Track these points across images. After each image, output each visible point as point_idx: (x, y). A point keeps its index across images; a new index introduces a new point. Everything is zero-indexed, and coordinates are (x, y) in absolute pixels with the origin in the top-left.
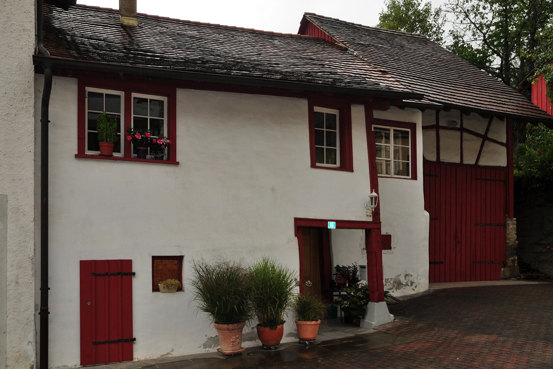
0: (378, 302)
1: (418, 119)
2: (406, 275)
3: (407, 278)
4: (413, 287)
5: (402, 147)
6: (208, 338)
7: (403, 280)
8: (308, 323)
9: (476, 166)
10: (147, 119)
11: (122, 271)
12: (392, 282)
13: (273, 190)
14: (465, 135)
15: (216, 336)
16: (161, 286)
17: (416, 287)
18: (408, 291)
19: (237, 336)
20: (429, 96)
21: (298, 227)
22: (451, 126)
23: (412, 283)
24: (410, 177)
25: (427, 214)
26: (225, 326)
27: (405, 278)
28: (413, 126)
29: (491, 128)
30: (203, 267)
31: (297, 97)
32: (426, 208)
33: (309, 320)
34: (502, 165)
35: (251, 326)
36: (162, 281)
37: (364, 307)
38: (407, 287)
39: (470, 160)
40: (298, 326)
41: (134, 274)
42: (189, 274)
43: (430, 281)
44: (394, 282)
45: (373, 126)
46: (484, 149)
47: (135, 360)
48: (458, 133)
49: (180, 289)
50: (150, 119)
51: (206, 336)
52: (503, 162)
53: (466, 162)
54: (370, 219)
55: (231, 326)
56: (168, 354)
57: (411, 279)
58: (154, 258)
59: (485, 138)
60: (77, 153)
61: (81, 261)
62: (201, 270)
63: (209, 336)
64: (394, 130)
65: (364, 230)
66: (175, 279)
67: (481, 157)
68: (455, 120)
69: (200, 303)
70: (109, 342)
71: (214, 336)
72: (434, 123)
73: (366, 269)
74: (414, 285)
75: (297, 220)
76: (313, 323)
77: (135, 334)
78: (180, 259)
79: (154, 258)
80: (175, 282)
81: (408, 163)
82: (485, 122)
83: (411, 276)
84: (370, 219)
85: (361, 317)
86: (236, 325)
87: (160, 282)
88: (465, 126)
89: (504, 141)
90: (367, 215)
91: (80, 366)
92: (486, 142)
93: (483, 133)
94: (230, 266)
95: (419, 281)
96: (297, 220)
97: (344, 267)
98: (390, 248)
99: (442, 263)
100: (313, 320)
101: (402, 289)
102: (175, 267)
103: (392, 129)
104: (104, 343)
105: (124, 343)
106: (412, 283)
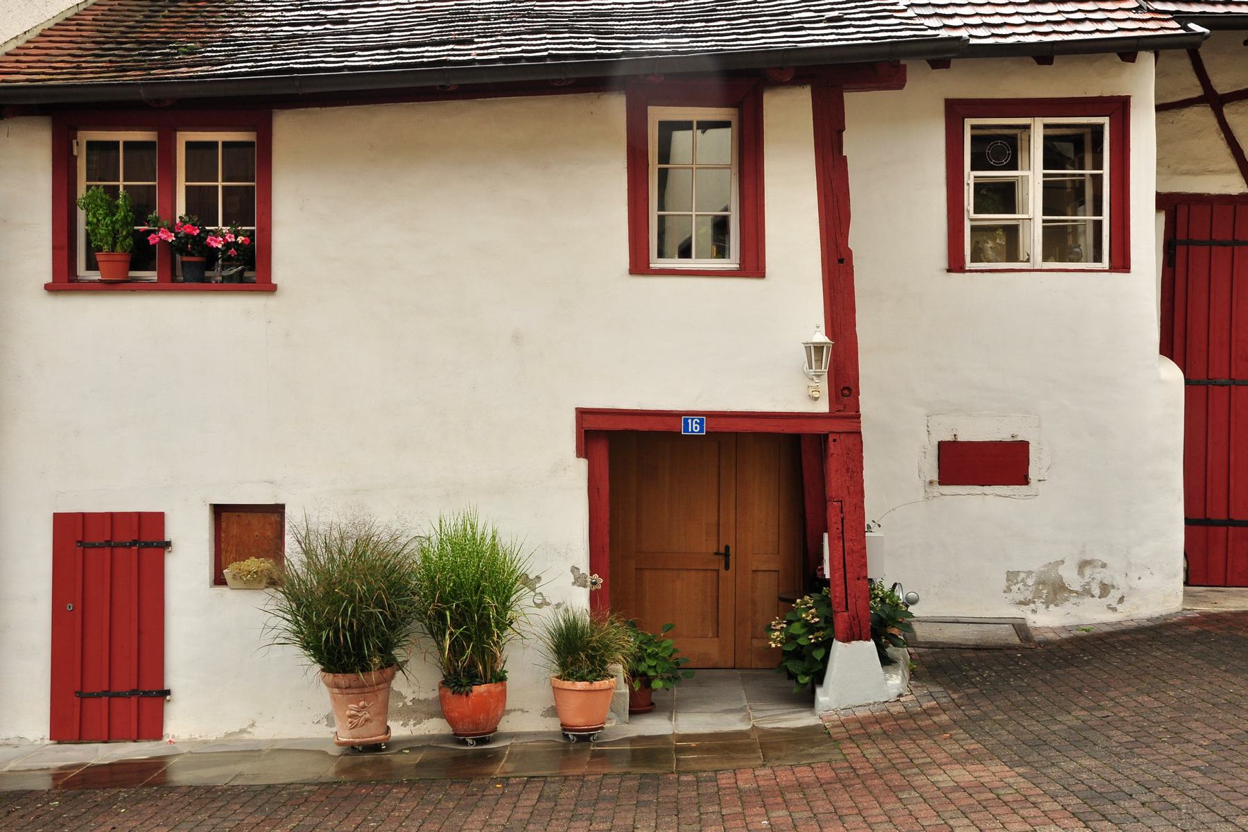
1: (1141, 84)
2: (1084, 565)
3: (1088, 571)
5: (1092, 175)
10: (223, 181)
11: (142, 537)
12: (1030, 582)
13: (517, 338)
17: (1121, 600)
18: (1094, 615)
19: (362, 704)
20: (856, 7)
23: (1105, 589)
24: (1105, 263)
25: (1172, 374)
28: (1119, 108)
31: (595, 91)
35: (417, 677)
38: (1088, 599)
41: (169, 544)
43: (1190, 580)
44: (1041, 582)
45: (969, 122)
47: (166, 739)
50: (223, 187)
56: (242, 731)
57: (1100, 575)
58: (219, 511)
60: (49, 280)
61: (56, 515)
70: (111, 695)
74: (1114, 595)
75: (582, 414)
77: (173, 679)
79: (219, 511)
80: (265, 564)
83: (1104, 566)
91: (48, 741)
94: (394, 529)
95: (1135, 583)
96: (582, 414)
98: (1025, 481)
100: (582, 679)
104: (99, 696)
105: (144, 701)
106: (1105, 589)
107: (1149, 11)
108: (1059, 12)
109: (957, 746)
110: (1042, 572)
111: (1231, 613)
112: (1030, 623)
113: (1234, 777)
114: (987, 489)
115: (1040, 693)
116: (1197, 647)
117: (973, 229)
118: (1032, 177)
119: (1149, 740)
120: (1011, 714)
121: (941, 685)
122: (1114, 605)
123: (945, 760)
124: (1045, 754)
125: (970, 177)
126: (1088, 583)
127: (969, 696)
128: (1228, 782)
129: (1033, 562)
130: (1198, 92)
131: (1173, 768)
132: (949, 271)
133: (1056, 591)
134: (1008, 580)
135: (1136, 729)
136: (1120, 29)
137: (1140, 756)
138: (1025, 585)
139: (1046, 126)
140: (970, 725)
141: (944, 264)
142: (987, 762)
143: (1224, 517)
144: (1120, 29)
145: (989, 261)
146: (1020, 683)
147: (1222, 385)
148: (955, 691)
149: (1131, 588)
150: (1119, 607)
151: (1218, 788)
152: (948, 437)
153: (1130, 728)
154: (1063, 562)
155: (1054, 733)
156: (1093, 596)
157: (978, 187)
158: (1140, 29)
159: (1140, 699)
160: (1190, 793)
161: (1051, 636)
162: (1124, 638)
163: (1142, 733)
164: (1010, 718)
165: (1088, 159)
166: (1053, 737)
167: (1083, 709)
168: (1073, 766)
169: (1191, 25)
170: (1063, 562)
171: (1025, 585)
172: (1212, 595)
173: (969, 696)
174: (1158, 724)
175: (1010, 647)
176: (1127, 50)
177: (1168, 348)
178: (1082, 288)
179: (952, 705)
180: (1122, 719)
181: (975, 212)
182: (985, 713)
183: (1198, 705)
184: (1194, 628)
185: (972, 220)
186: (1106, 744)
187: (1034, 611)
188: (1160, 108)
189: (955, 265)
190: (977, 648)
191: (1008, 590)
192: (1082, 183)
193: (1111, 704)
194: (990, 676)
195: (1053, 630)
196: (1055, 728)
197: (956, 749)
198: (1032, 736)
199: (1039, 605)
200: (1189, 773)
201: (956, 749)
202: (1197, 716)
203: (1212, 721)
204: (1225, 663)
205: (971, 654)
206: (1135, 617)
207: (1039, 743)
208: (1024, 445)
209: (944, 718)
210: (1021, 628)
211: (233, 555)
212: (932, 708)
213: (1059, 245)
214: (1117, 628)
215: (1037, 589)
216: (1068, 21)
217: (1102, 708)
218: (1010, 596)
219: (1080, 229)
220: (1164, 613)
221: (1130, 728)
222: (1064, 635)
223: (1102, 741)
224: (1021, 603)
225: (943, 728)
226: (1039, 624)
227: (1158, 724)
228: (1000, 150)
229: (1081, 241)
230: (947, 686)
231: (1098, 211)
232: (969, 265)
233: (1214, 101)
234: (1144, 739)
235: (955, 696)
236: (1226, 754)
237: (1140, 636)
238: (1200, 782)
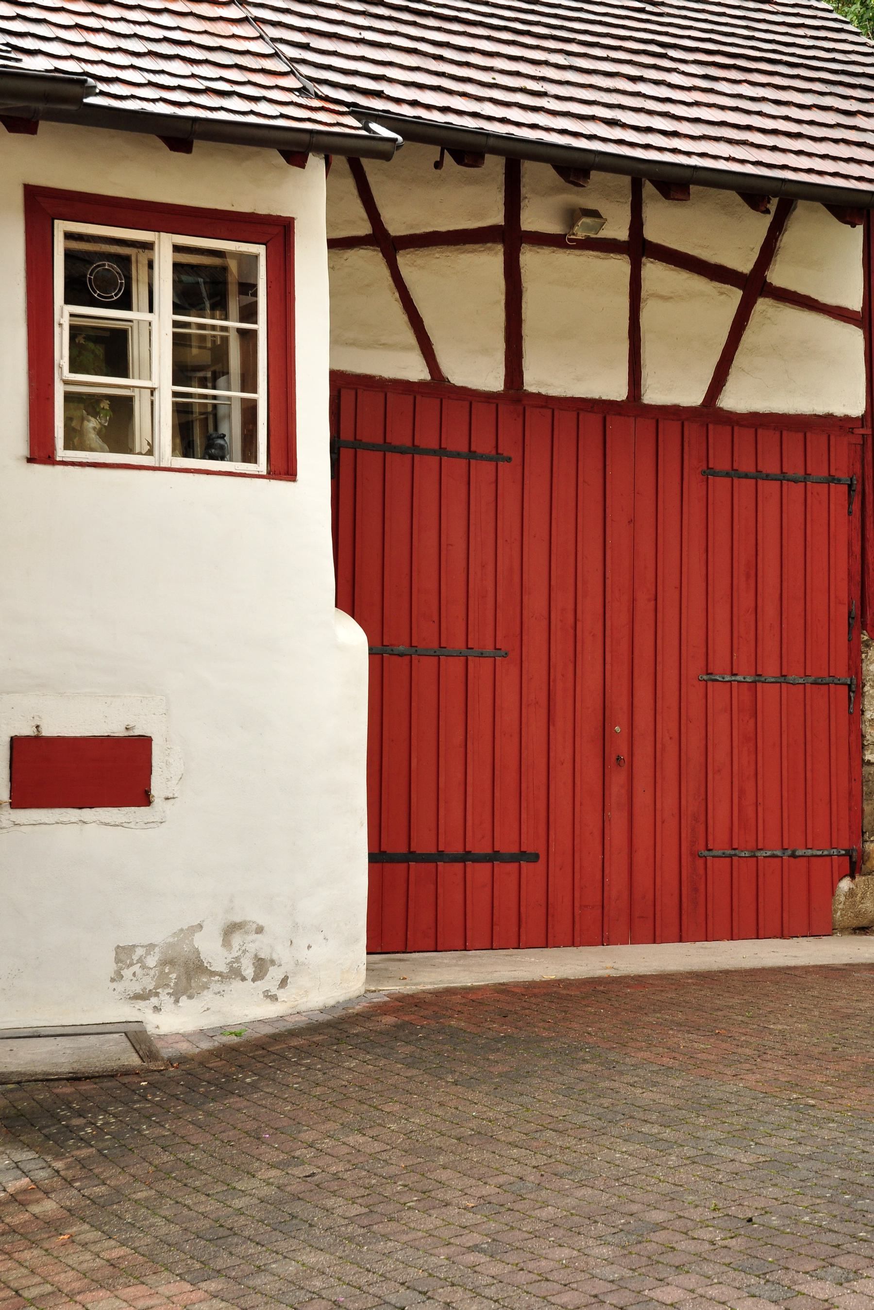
1: (309, 200)
2: (231, 929)
3: (237, 940)
4: (270, 982)
7: (211, 949)
9: (709, 412)
12: (152, 961)
14: (654, 273)
17: (284, 982)
18: (245, 1008)
20: (379, 94)
22: (580, 233)
23: (261, 966)
24: (262, 465)
25: (352, 637)
27: (226, 943)
28: (278, 233)
29: (788, 239)
34: (839, 410)
38: (237, 984)
39: (675, 386)
44: (167, 962)
45: (61, 227)
46: (748, 338)
48: (621, 266)
52: (849, 398)
53: (652, 396)
57: (256, 945)
59: (754, 286)
64: (177, 249)
67: (733, 371)
68: (591, 205)
72: (497, 218)
74: (274, 974)
82: (758, 226)
83: (260, 930)
88: (652, 233)
89: (855, 301)
92: (763, 305)
93: (745, 266)
98: (145, 799)
99: (534, 858)
101: (207, 995)
103: (164, 247)
106: (261, 966)
107: (317, 97)
108: (193, 76)
109: (88, 1256)
110: (170, 945)
111: (430, 992)
112: (150, 1029)
113: (535, 1257)
114: (87, 814)
115: (195, 1146)
116: (403, 1050)
117: (69, 397)
118: (155, 327)
119: (390, 1208)
120: (160, 1186)
121: (30, 1147)
122: (274, 991)
123: (77, 1285)
124: (241, 1250)
125: (63, 313)
126: (237, 959)
127: (82, 1163)
128: (531, 1265)
129: (155, 930)
130: (364, 229)
131: (443, 1252)
132: (30, 460)
133: (188, 974)
134: (118, 960)
135: (363, 1192)
136: (282, 116)
137: (386, 1237)
138: (144, 967)
139: (177, 249)
140: (98, 1212)
141: (22, 448)
142: (151, 1279)
143: (403, 850)
144: (282, 116)
145: (92, 450)
146: (158, 1131)
147: (400, 655)
148: (58, 1156)
149: (297, 963)
150: (281, 994)
151: (522, 1278)
152: (27, 730)
153: (352, 1191)
154: (200, 926)
155: (240, 1212)
156: (244, 979)
157: (75, 331)
158: (309, 120)
159: (351, 1140)
160: (487, 1292)
161: (184, 1047)
162: (294, 1042)
163: (375, 1198)
164: (161, 1194)
165: (233, 307)
166: (242, 1220)
167: (272, 1166)
168: (292, 1268)
169: (374, 126)
170: (200, 926)
171: (144, 967)
172: (393, 966)
173: (82, 1163)
174: (393, 1178)
175: (127, 1072)
176: (295, 148)
177: (348, 599)
178: (226, 498)
179: (57, 1182)
180: (336, 1177)
181: (73, 369)
182: (117, 1190)
183: (437, 1142)
184: (390, 1020)
185: (66, 383)
186: (328, 1223)
187: (157, 1009)
188: (333, 244)
189: (40, 452)
190: (75, 1078)
191: (118, 977)
192: (225, 340)
193: (310, 1154)
194: (107, 1123)
195: (185, 1037)
196: (238, 1203)
197: (85, 1260)
198: (207, 1223)
199: (165, 999)
200: (471, 1258)
201: (85, 1260)
202: (442, 1159)
203: (465, 1165)
204: (453, 1072)
205: (66, 1089)
206: (302, 1008)
207: (222, 1235)
208: (145, 742)
209: (48, 1207)
210: (137, 1038)
212: (25, 1191)
213: (198, 434)
214: (281, 1027)
215: (162, 972)
216: (207, 91)
217: (299, 1161)
218: (120, 986)
219: (222, 411)
220: (341, 999)
221: (352, 1191)
222: (206, 1045)
223: (318, 1216)
224: (138, 997)
225: (53, 1226)
226: (164, 1030)
227: (393, 1178)
228: (102, 278)
229: (224, 429)
230: (41, 1149)
231: (249, 382)
232: (61, 453)
233: (388, 245)
234: (380, 1208)
235: (59, 1165)
236: (507, 1218)
237: (318, 1038)
238: (493, 1271)
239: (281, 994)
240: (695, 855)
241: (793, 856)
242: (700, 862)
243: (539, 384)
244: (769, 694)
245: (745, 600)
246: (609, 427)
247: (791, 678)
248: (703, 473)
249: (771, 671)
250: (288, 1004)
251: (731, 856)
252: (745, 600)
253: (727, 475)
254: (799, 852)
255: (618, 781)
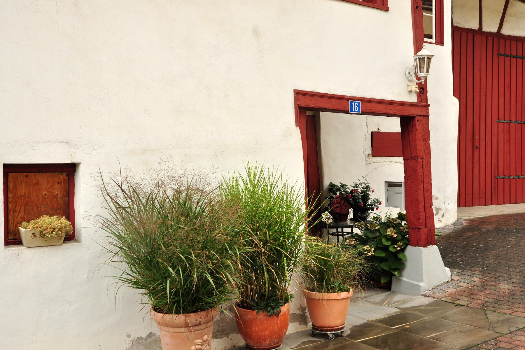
0: (425, 246)
6: (133, 341)
8: (334, 296)
9: (498, 35)
13: (256, 32)
15: (150, 335)
16: (24, 231)
17: (443, 216)
21: (300, 108)
24: (434, 40)
25: (456, 101)
26: (180, 318)
30: (125, 187)
32: (457, 92)
33: (333, 290)
36: (29, 221)
37: (400, 256)
39: (490, 26)
40: (310, 300)
42: (88, 202)
46: (508, 11)
49: (70, 237)
51: (129, 336)
53: (485, 29)
54: (414, 99)
55: (193, 318)
58: (8, 168)
62: (120, 194)
63: (134, 336)
65: (398, 119)
66: (60, 215)
67: (504, 24)
69: (122, 267)
71: (144, 334)
73: (402, 189)
76: (343, 295)
78: (69, 170)
80: (57, 222)
81: (431, 17)
84: (414, 99)
85: (396, 273)
86: (203, 314)
87: (24, 223)
90: (410, 92)
97: (343, 186)
100: (341, 290)
102: (58, 191)
152: (376, 130)
211: (22, 214)
239: (443, 220)
240: (495, 178)
241: (519, 178)
242: (496, 180)
243: (457, 23)
244: (513, 126)
245: (507, 97)
246: (475, 38)
247: (518, 122)
248: (498, 54)
249: (513, 119)
250: (445, 223)
251: (504, 178)
252: (507, 97)
253: (504, 56)
254: (520, 177)
255: (476, 153)
